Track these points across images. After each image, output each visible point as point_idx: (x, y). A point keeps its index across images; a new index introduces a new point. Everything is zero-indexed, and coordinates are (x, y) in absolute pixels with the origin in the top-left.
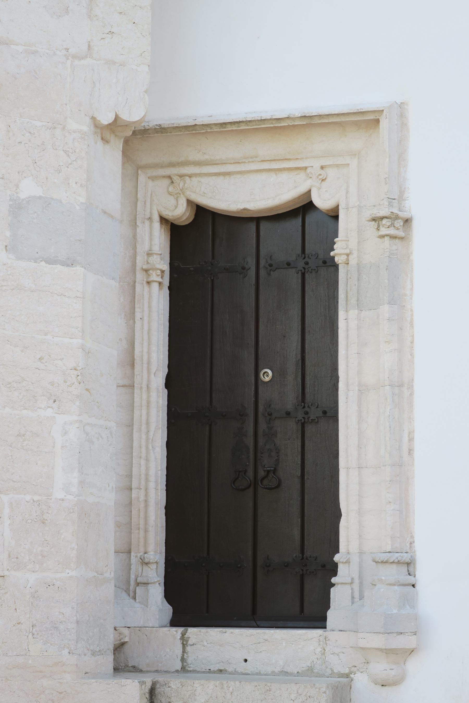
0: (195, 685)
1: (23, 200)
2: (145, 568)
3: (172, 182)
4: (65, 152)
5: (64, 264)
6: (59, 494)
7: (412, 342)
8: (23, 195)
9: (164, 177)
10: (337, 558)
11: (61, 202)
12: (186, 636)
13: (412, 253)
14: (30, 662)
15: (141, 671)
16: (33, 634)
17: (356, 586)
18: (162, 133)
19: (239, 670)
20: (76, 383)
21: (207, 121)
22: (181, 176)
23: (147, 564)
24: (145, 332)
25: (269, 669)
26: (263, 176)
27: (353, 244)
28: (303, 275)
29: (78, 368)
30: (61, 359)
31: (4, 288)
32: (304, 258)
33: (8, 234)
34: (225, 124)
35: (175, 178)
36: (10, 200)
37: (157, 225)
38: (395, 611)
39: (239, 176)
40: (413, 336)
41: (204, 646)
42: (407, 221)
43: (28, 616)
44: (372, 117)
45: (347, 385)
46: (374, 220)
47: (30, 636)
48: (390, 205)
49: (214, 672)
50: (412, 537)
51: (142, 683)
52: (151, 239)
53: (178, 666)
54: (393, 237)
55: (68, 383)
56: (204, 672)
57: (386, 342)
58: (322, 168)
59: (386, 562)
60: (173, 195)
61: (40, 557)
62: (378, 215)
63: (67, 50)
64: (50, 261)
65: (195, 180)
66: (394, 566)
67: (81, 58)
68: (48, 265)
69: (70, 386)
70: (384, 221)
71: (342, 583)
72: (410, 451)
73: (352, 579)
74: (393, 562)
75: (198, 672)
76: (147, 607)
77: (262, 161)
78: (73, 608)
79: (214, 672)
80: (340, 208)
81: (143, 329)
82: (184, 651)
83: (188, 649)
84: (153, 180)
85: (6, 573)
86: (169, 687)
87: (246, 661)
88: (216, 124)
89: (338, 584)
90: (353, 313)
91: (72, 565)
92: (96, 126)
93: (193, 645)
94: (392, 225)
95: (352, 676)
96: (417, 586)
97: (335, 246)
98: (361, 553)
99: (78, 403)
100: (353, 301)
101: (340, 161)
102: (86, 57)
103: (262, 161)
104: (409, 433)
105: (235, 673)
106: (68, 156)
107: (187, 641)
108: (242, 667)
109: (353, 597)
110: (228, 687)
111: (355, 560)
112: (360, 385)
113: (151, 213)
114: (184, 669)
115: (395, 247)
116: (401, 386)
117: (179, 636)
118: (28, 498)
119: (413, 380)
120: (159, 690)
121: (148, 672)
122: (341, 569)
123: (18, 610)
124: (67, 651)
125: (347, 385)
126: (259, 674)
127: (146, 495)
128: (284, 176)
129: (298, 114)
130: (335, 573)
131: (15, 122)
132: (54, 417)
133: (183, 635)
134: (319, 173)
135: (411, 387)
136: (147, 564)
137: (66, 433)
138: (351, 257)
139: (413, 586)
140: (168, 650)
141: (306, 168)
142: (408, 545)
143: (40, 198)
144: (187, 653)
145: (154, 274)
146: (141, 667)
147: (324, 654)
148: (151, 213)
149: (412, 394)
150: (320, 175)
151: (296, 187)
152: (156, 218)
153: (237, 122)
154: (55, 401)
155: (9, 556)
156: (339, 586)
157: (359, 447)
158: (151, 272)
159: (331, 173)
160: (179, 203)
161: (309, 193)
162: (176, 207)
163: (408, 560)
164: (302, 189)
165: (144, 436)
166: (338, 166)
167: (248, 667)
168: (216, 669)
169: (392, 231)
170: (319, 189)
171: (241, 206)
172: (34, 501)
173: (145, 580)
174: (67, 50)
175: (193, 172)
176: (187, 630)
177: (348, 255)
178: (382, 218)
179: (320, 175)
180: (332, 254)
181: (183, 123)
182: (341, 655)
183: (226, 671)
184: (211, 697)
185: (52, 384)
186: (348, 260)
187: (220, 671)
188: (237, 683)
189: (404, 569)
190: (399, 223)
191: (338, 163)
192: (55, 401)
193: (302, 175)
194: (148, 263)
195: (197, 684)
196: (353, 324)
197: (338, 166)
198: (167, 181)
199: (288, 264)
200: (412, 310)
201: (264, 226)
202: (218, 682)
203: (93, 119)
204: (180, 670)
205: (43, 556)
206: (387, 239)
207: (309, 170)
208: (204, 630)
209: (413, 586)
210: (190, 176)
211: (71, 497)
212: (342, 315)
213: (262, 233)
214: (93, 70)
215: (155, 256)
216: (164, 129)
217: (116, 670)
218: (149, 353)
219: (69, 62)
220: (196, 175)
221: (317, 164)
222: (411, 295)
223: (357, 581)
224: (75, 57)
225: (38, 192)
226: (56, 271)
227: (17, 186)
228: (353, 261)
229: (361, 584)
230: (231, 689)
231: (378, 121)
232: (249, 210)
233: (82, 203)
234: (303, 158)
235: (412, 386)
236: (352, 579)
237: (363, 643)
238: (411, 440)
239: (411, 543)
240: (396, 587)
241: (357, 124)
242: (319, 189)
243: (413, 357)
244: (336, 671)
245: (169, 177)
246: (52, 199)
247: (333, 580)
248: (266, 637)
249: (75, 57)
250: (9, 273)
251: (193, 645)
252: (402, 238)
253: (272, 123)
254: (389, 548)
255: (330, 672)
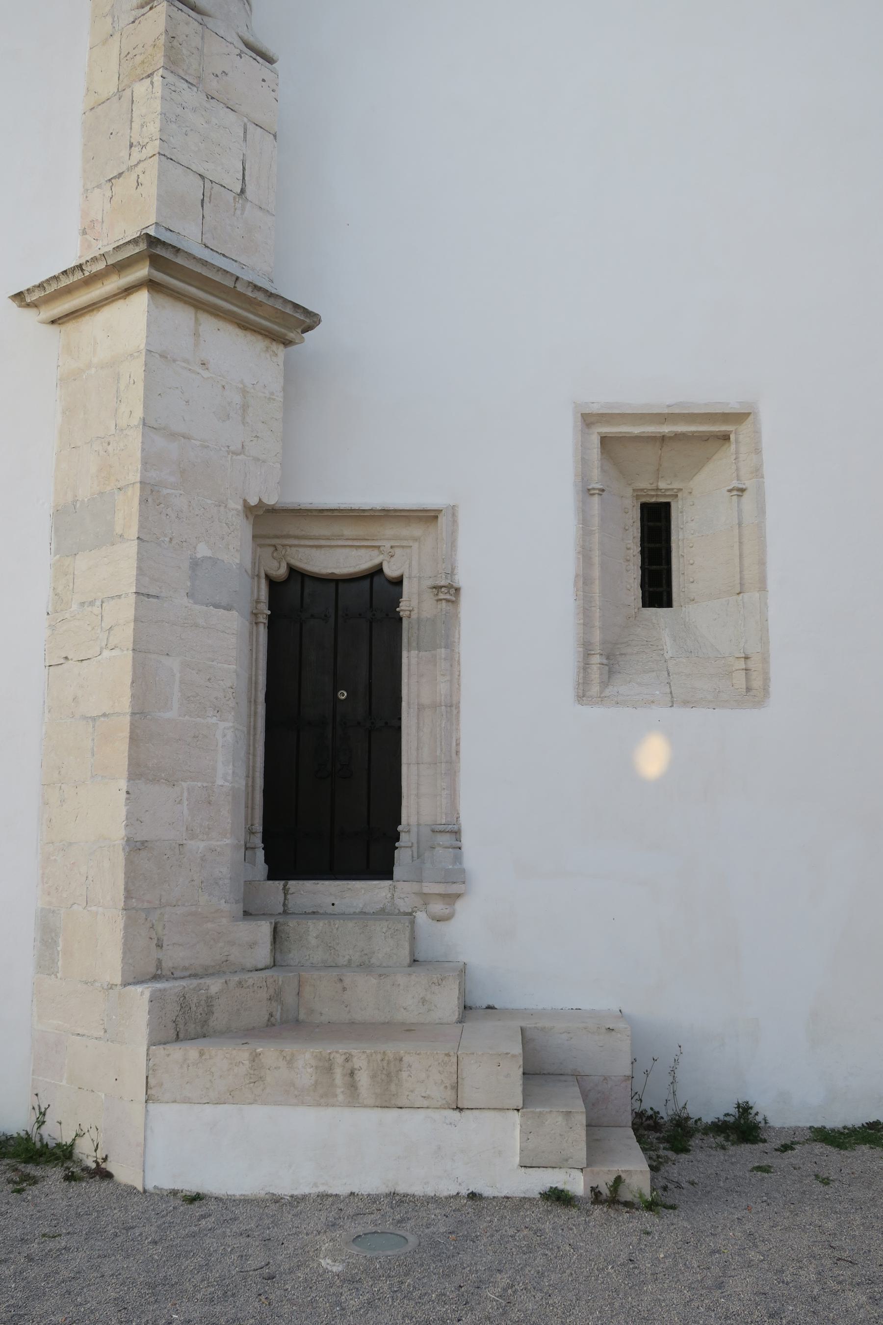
0: (309, 924)
1: (199, 559)
2: (252, 836)
3: (276, 549)
4: (227, 524)
5: (225, 608)
6: (220, 782)
7: (459, 676)
8: (199, 556)
9: (270, 545)
10: (400, 828)
11: (223, 561)
12: (287, 887)
13: (459, 613)
14: (200, 910)
15: (251, 914)
16: (202, 889)
17: (415, 849)
18: (273, 513)
19: (329, 911)
20: (232, 698)
21: (309, 507)
22: (284, 546)
23: (253, 833)
24: (254, 660)
25: (352, 910)
26: (347, 550)
27: (414, 603)
28: (371, 623)
29: (234, 687)
30: (223, 680)
31: (186, 625)
32: (372, 611)
33: (189, 584)
34: (323, 510)
35: (279, 547)
36: (191, 558)
37: (263, 582)
38: (450, 867)
39: (328, 549)
40: (460, 671)
41: (301, 894)
42: (457, 590)
43: (199, 875)
44: (433, 514)
45: (409, 704)
46: (434, 587)
47: (200, 890)
48: (446, 578)
49: (309, 914)
50: (458, 814)
51: (271, 923)
52: (259, 591)
53: (281, 910)
54: (448, 601)
55: (227, 699)
56: (301, 914)
57: (442, 675)
58: (392, 547)
59: (443, 832)
60: (277, 560)
61: (207, 830)
62: (439, 584)
63: (228, 447)
64: (217, 606)
65: (294, 549)
66: (448, 834)
67: (238, 454)
68: (215, 609)
69: (228, 700)
70: (443, 589)
71: (405, 847)
72: (457, 753)
73: (412, 843)
74: (448, 832)
75: (297, 914)
76: (255, 865)
77: (347, 539)
78: (228, 868)
79: (309, 914)
80: (404, 577)
81: (252, 657)
82: (285, 899)
83: (289, 897)
84: (260, 547)
85: (185, 842)
86: (288, 926)
87: (333, 904)
88: (316, 510)
89: (401, 847)
90: (414, 653)
91: (228, 835)
92: (245, 506)
93: (293, 893)
94: (449, 592)
95: (414, 914)
96: (463, 849)
97: (401, 604)
98: (419, 825)
99: (233, 714)
100: (414, 644)
101: (405, 543)
102: (241, 454)
103: (347, 539)
104: (457, 740)
105: (326, 914)
106: (229, 527)
107: (288, 891)
108: (330, 909)
109: (413, 857)
110: (335, 924)
111: (414, 830)
112: (418, 705)
113: (259, 571)
114: (285, 912)
115: (448, 608)
116: (451, 706)
117: (281, 887)
118: (199, 784)
119: (459, 702)
120: (280, 928)
121: (256, 915)
122: (403, 836)
123: (192, 871)
124: (223, 900)
125: (409, 704)
126: (344, 914)
127: (253, 782)
128: (362, 552)
129: (379, 508)
130: (398, 839)
131: (194, 499)
132: (217, 724)
133: (285, 886)
134: (390, 551)
135: (458, 707)
136: (253, 833)
137: (225, 736)
138: (412, 613)
139: (460, 848)
140: (272, 898)
141: (379, 547)
142: (455, 819)
143: (210, 558)
144: (288, 900)
145: (261, 617)
146: (250, 911)
147: (393, 898)
148: (259, 571)
149: (458, 712)
150: (390, 552)
151: (371, 560)
152: (263, 575)
153: (332, 510)
154: (218, 712)
155: (187, 829)
156: (402, 849)
157: (418, 749)
158: (259, 615)
159: (398, 551)
160: (282, 565)
161: (381, 564)
162: (279, 568)
163: (457, 830)
164: (376, 561)
165: (252, 738)
166: (403, 547)
167: (336, 909)
168: (310, 911)
169: (448, 597)
170: (389, 562)
171: (330, 571)
172: (203, 787)
173: (253, 846)
174: (228, 447)
175: (293, 543)
176: (287, 883)
177: (410, 611)
178: (441, 587)
179: (390, 552)
180: (398, 609)
181: (291, 506)
182: (406, 899)
183: (318, 912)
184: (321, 932)
185: (216, 698)
186: (410, 615)
187: (314, 913)
188: (342, 921)
189: (453, 836)
190: (452, 591)
191: (404, 545)
192: (218, 712)
193: (376, 552)
194: (256, 609)
195: (310, 923)
196: (414, 661)
197: (403, 547)
198: (272, 549)
199: (360, 615)
200: (459, 653)
201: (341, 585)
202: (327, 921)
203: (245, 501)
204: (282, 912)
205: (209, 829)
206: (443, 601)
207: (382, 549)
208: (301, 882)
209: (460, 848)
210: (290, 546)
211: (227, 784)
212: (405, 654)
213: (340, 591)
214: (245, 464)
215: (262, 604)
216: (275, 510)
217: (247, 914)
218: (256, 675)
219: (230, 456)
220: (296, 546)
221: (388, 544)
222: (459, 642)
223: (415, 845)
224: (234, 453)
225: (209, 553)
226: (220, 614)
227: (195, 548)
228: (414, 615)
229: (418, 847)
230: (337, 926)
231: (436, 517)
232: (335, 574)
233: (237, 564)
234: (378, 539)
235: (459, 706)
236: (412, 843)
237: (426, 890)
238: (458, 744)
239: (457, 818)
240: (450, 850)
241: (420, 519)
242: (389, 562)
243: (460, 686)
244: (402, 911)
245: (275, 546)
246: (218, 559)
247: (397, 844)
248: (349, 887)
249: (234, 453)
250: (189, 613)
251: (293, 893)
252: (453, 602)
253: (358, 513)
254: (444, 821)
255: (397, 911)
